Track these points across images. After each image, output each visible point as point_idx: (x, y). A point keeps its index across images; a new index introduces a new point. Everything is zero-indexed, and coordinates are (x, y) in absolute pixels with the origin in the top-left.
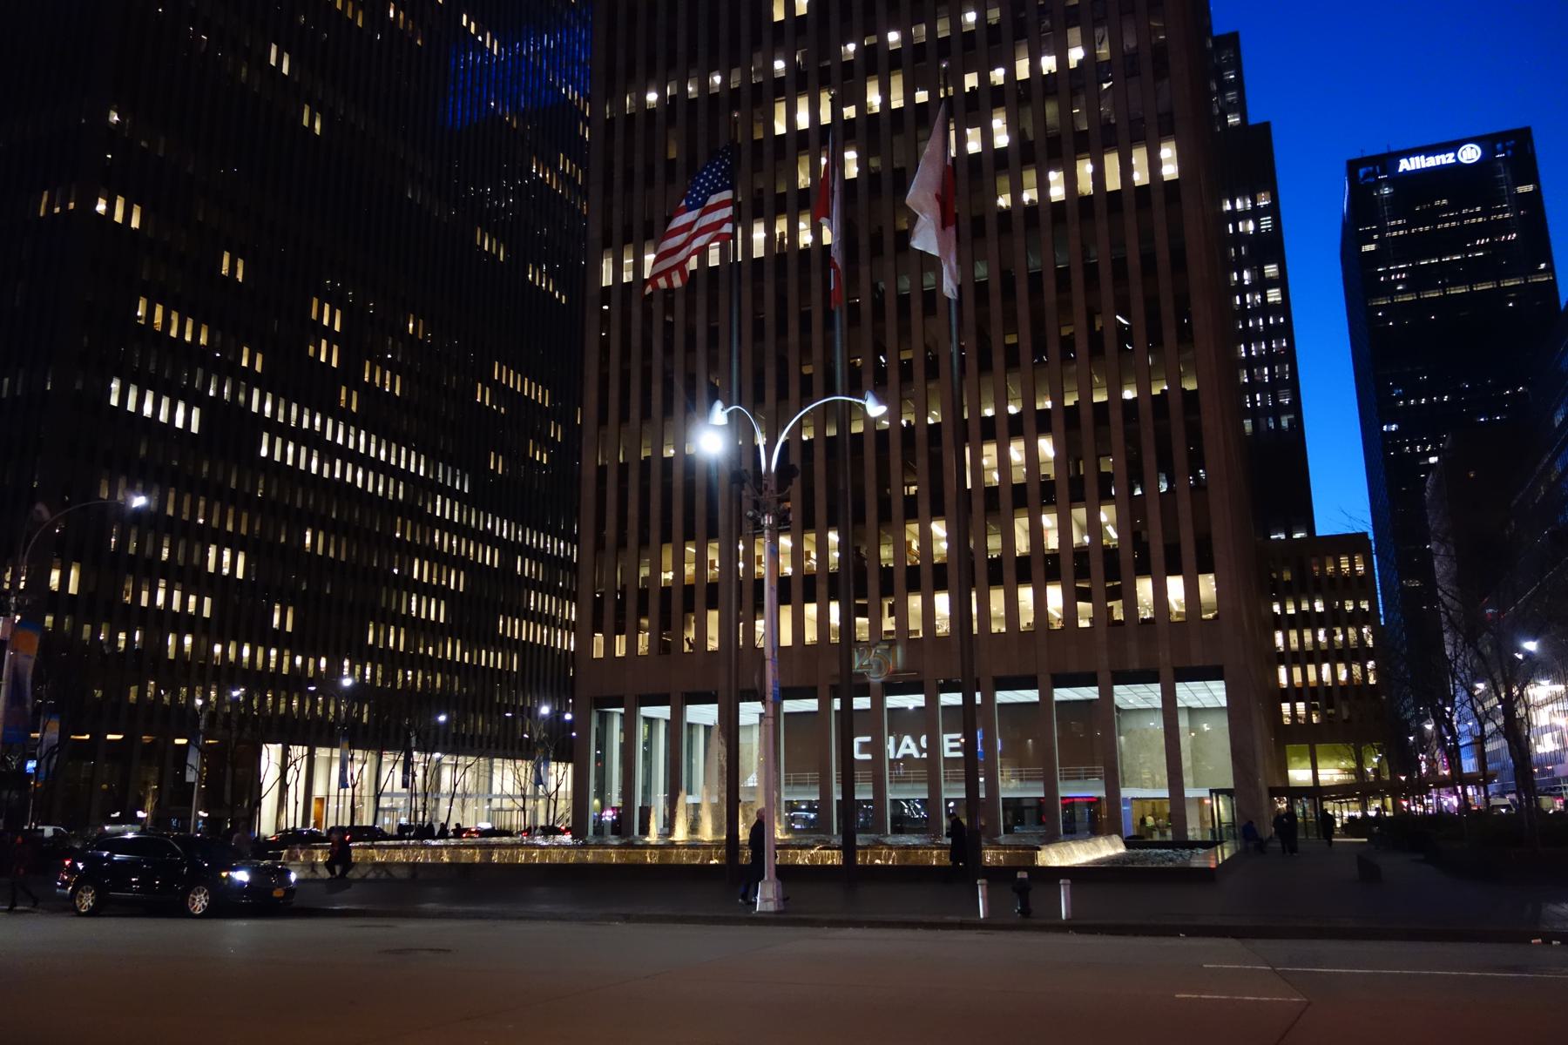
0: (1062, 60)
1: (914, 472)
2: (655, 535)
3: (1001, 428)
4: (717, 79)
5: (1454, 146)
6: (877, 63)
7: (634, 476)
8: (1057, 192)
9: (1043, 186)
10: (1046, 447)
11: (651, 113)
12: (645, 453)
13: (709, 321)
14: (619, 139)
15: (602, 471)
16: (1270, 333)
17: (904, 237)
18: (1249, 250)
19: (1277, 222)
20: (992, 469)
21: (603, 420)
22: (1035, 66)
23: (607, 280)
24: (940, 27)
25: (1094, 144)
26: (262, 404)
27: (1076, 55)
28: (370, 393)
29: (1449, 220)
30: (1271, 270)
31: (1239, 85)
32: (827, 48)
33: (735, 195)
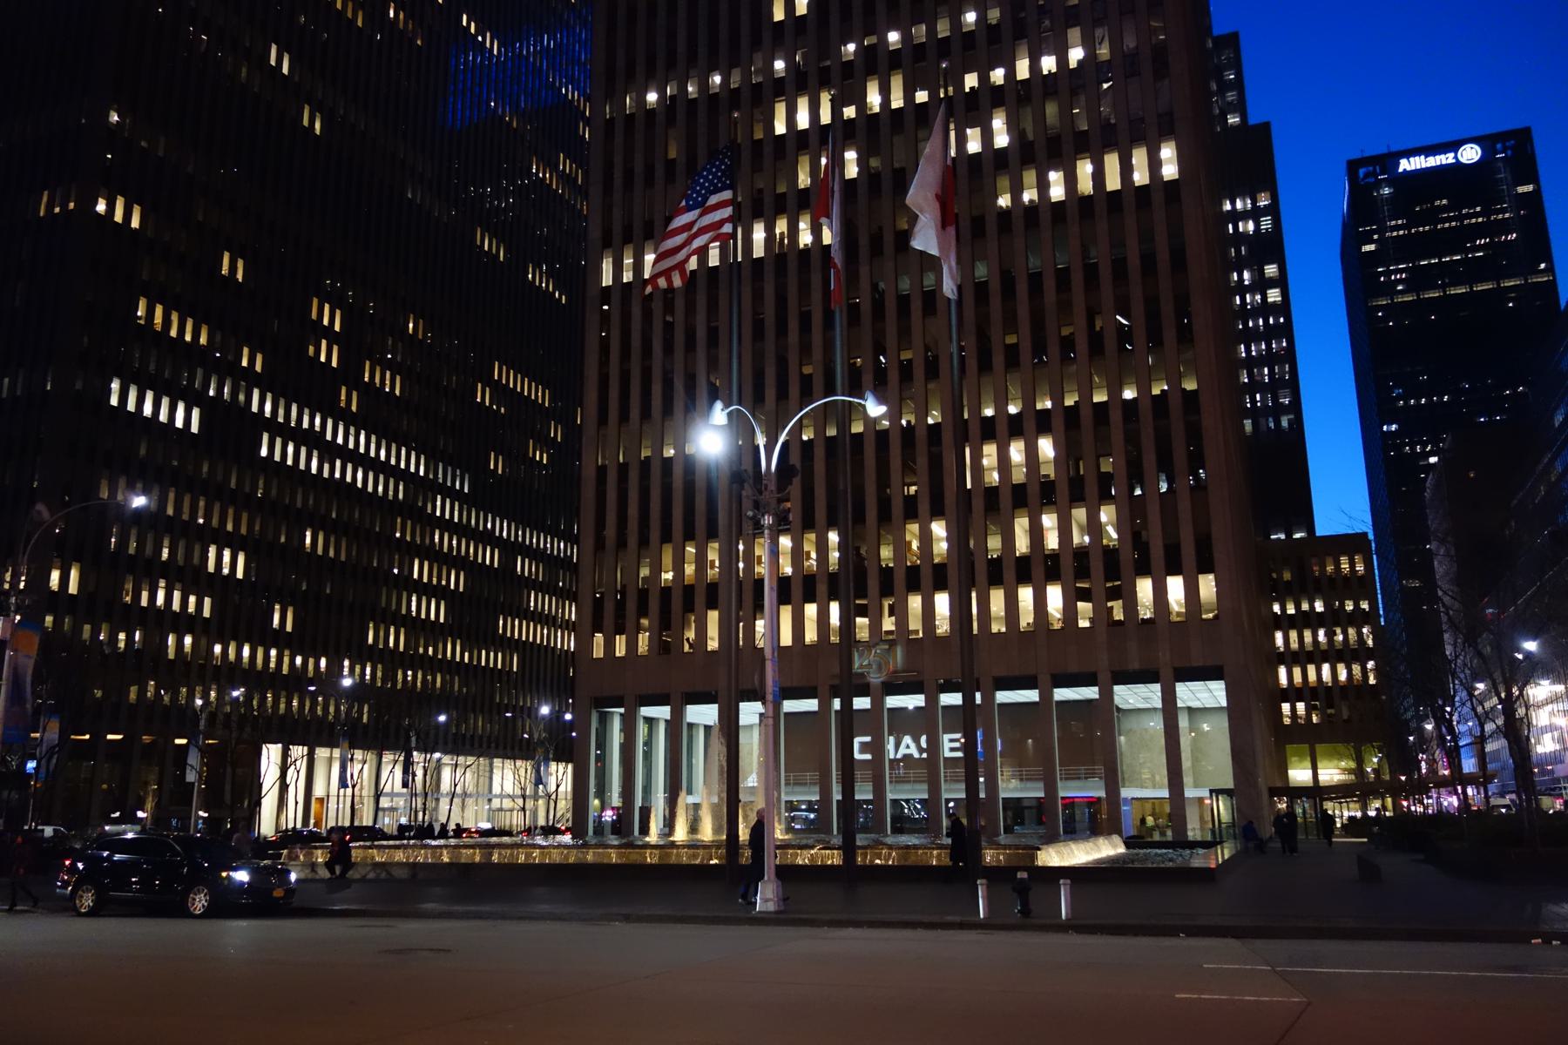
0: (1062, 60)
1: (914, 472)
2: (655, 535)
3: (1001, 428)
4: (717, 79)
5: (1454, 146)
6: (877, 63)
7: (634, 476)
8: (1057, 192)
9: (1043, 186)
10: (1046, 447)
11: (651, 113)
12: (645, 453)
13: (709, 321)
14: (619, 139)
15: (602, 471)
16: (1270, 333)
17: (904, 237)
18: (1249, 250)
19: (1277, 222)
20: (992, 469)
21: (603, 420)
22: (1035, 66)
23: (607, 280)
24: (940, 27)
25: (1094, 144)
26: (262, 404)
27: (1076, 55)
28: (370, 393)
29: (1449, 220)
30: (1271, 270)
31: (1239, 85)
32: (827, 48)
33: (735, 195)
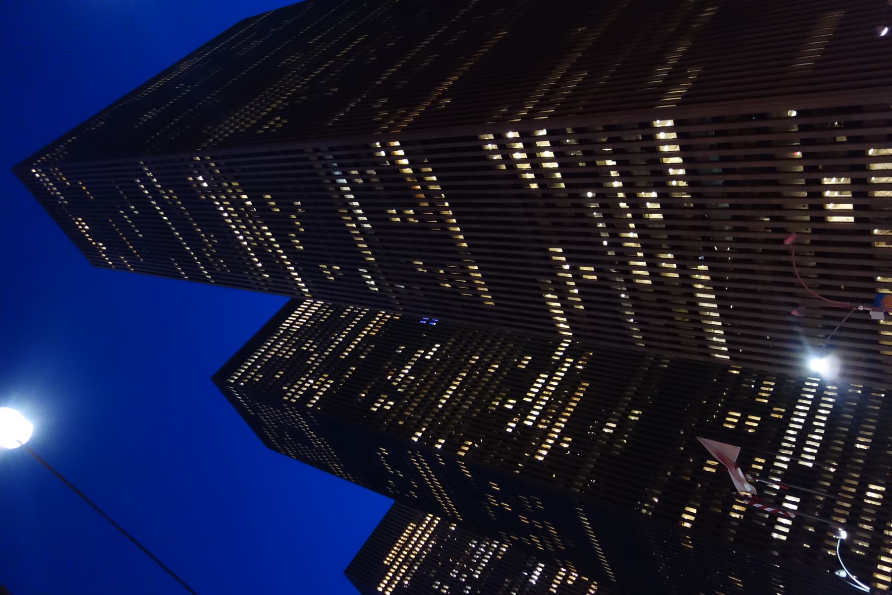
4: (623, 296)
26: (783, 462)
28: (774, 399)
